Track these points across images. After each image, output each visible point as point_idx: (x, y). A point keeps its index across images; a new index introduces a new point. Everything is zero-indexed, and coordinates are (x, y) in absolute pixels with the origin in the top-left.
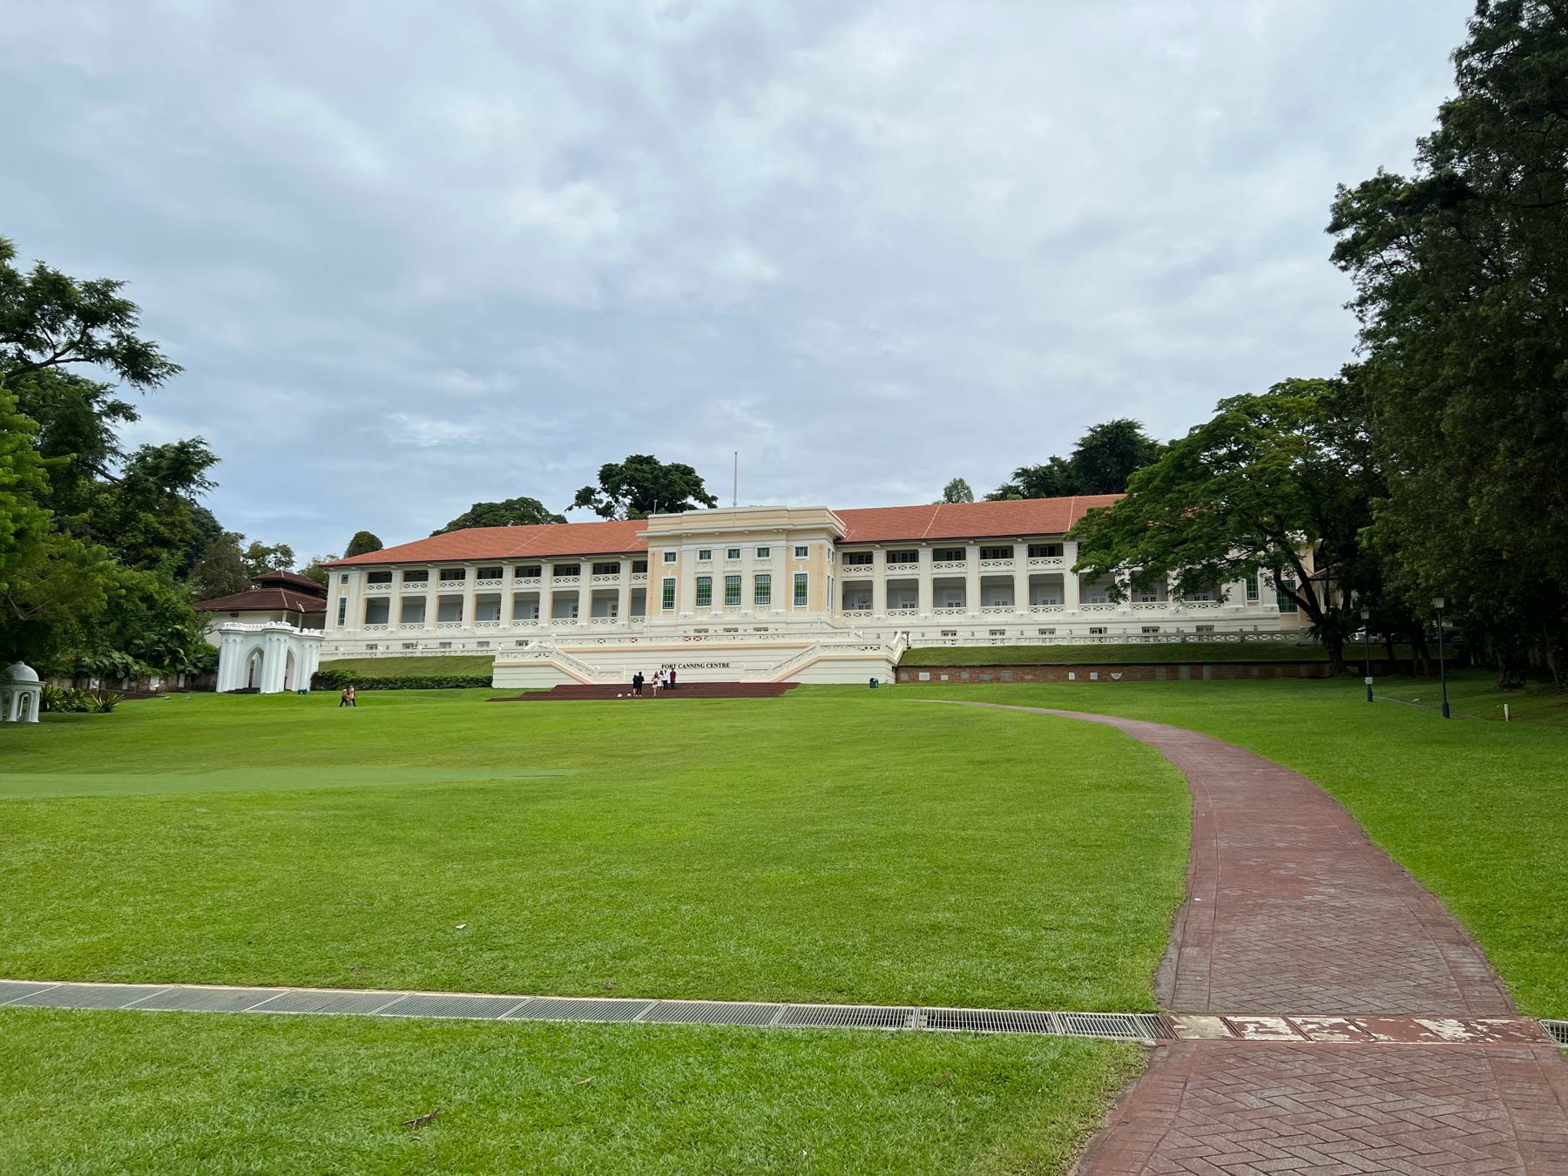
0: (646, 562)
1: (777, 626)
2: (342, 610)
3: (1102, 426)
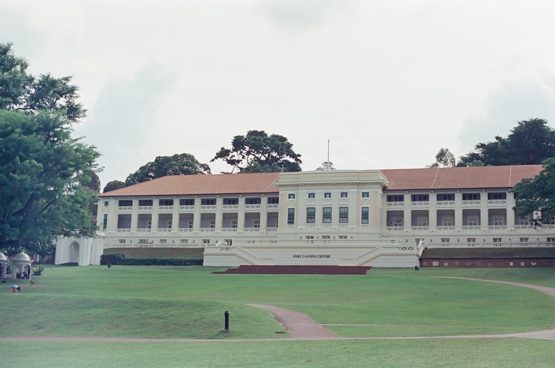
0: (278, 197)
1: (352, 235)
2: (105, 221)
3: (525, 122)
